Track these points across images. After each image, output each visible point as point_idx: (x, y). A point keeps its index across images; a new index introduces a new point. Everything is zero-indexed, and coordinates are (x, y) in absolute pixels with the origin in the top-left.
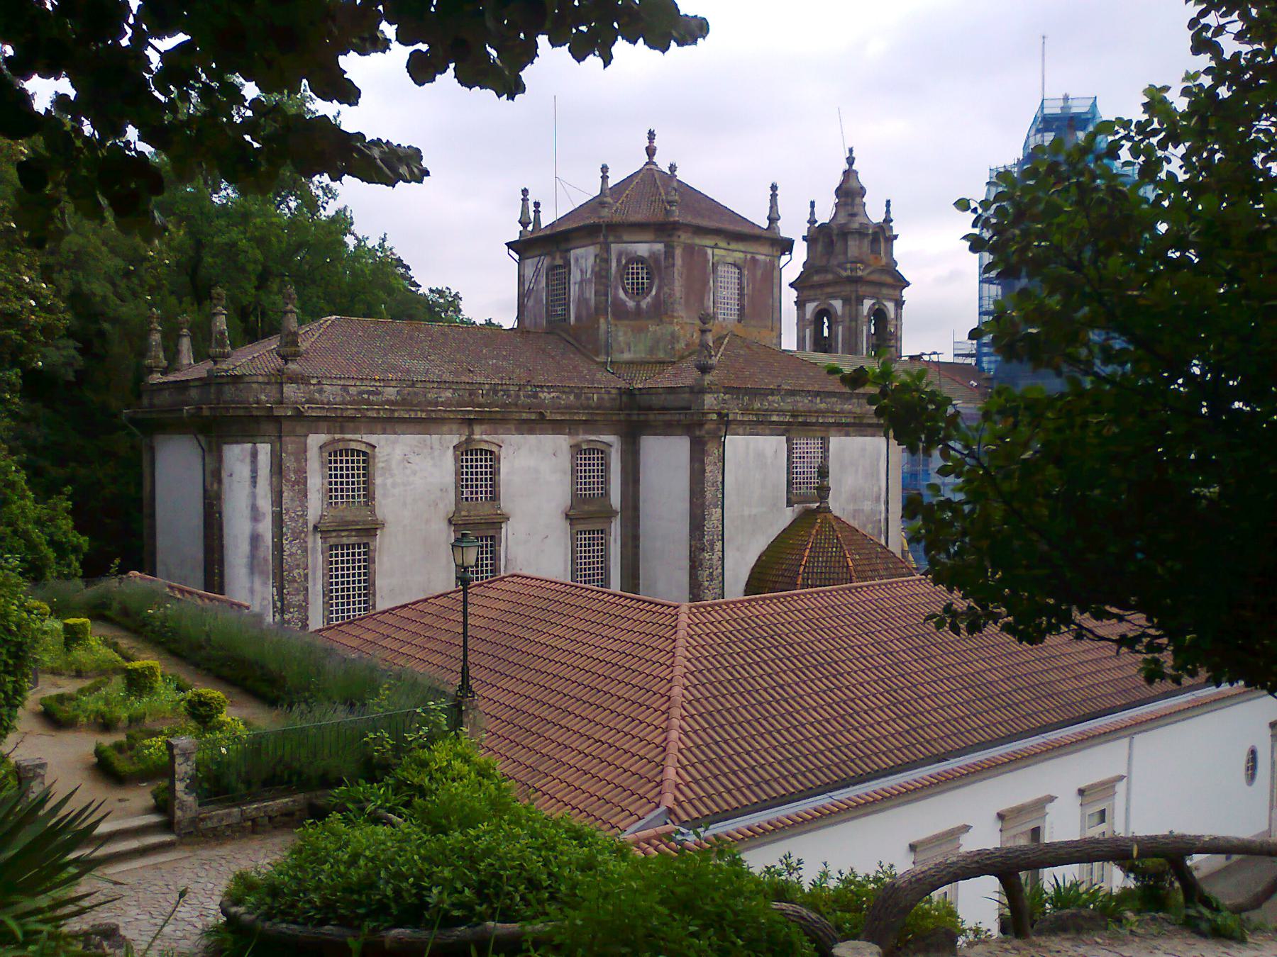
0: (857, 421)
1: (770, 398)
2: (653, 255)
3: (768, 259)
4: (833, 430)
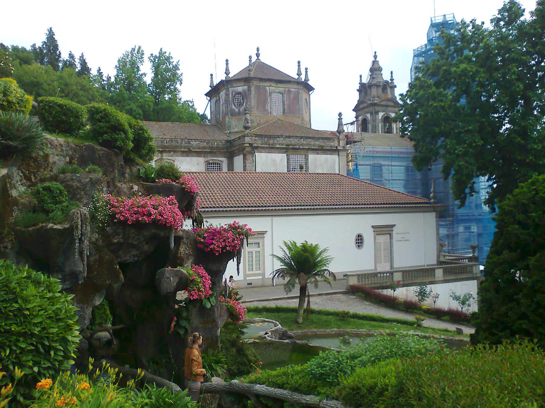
0: (320, 148)
1: (278, 139)
2: (244, 90)
3: (296, 90)
4: (310, 152)
